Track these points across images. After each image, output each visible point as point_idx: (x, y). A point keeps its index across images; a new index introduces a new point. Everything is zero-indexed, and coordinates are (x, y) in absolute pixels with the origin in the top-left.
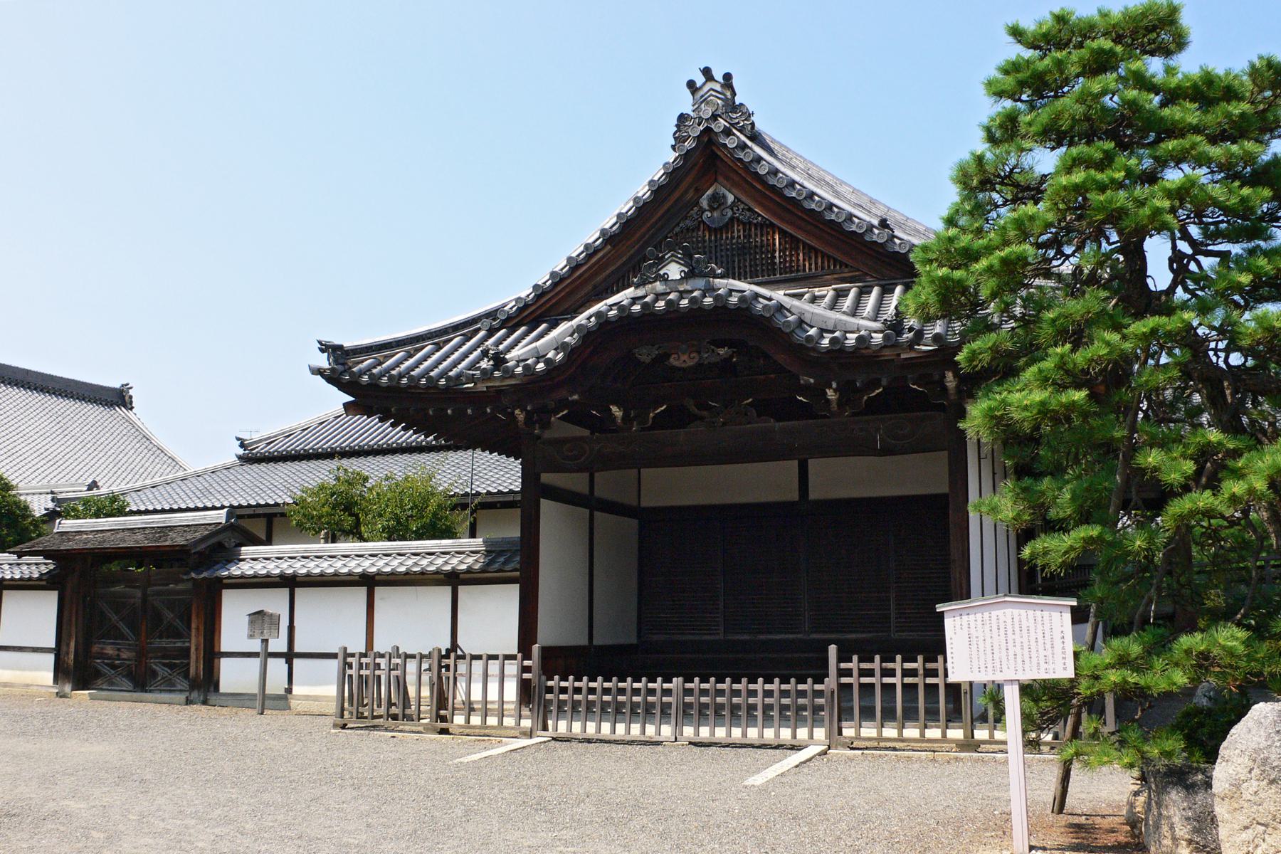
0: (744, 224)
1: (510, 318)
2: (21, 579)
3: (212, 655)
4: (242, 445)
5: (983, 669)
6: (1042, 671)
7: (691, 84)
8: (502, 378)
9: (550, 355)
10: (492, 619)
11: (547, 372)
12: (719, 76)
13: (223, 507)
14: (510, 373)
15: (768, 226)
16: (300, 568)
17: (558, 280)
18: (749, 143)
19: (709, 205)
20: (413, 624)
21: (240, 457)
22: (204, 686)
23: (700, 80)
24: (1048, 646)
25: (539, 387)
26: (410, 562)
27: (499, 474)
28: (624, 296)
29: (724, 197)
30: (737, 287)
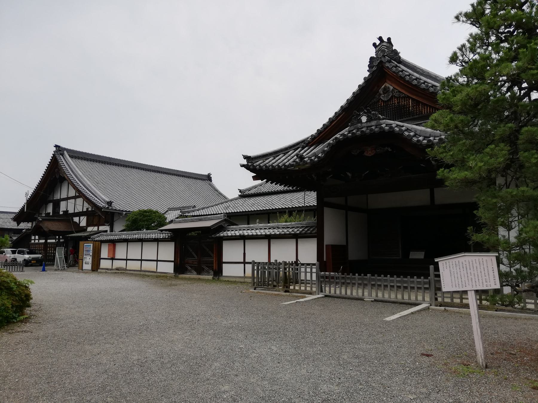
0: (397, 98)
1: (309, 142)
2: (163, 238)
3: (220, 263)
4: (240, 192)
5: (457, 285)
6: (485, 286)
7: (374, 45)
8: (304, 165)
9: (320, 155)
10: (308, 252)
11: (319, 161)
12: (385, 40)
13: (221, 214)
14: (306, 163)
15: (407, 98)
16: (246, 233)
17: (325, 126)
18: (398, 65)
19: (383, 92)
20: (284, 252)
21: (240, 196)
22: (218, 272)
23: (378, 42)
24: (487, 274)
25: (317, 166)
26: (301, 230)
27: (310, 198)
28: (345, 131)
29: (389, 88)
30: (387, 123)
